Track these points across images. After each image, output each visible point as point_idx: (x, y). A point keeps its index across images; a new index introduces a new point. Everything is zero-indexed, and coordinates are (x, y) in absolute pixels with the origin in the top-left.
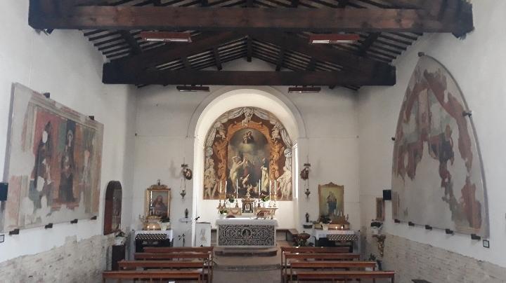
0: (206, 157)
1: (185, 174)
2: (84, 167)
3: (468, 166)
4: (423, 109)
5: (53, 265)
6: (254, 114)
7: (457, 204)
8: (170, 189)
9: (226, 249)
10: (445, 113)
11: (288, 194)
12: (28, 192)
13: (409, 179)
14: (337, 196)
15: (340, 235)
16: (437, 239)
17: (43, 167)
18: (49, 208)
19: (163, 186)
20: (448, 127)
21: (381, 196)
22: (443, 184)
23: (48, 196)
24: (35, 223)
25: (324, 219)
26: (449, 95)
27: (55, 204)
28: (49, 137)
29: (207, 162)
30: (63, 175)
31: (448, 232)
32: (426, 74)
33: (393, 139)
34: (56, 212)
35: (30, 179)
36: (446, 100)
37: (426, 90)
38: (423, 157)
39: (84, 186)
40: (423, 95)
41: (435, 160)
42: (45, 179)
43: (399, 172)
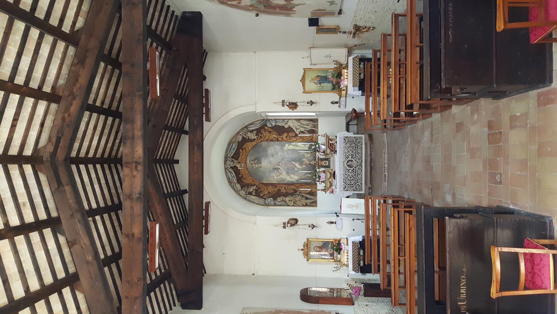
0: (275, 205)
6: (232, 157)
8: (308, 239)
9: (366, 184)
11: (311, 123)
14: (314, 75)
15: (353, 65)
19: (304, 246)
21: (314, 28)
25: (337, 87)
33: (257, 15)
43: (291, 9)
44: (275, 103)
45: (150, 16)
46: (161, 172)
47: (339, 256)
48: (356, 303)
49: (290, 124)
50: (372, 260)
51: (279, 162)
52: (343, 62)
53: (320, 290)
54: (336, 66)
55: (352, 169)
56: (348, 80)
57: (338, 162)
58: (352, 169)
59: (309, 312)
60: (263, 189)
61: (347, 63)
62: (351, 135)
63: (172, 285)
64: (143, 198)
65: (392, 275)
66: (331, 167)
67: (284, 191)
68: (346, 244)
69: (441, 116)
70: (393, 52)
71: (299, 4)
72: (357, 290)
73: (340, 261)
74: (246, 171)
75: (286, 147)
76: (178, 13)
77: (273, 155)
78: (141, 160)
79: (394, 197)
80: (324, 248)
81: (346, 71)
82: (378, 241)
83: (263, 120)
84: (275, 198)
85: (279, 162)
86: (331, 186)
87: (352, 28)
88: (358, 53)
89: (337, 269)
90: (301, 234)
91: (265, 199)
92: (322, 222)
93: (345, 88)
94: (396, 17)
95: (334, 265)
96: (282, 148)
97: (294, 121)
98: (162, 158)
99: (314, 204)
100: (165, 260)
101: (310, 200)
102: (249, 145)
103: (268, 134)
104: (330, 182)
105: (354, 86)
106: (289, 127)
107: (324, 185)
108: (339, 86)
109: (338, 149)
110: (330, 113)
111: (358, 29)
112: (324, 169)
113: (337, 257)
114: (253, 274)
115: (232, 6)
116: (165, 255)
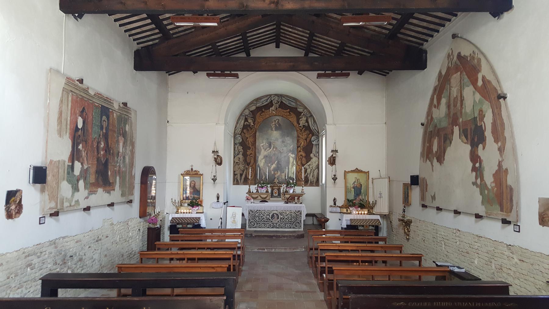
0: (235, 144)
1: (216, 160)
2: (119, 152)
3: (501, 150)
4: (455, 92)
5: (92, 245)
6: (282, 102)
7: (487, 189)
8: (202, 175)
9: (255, 231)
10: (478, 96)
11: (315, 180)
12: (66, 175)
13: (438, 164)
14: (363, 182)
15: (372, 220)
16: (466, 223)
17: (79, 151)
18: (87, 191)
19: (195, 171)
20: (481, 111)
21: (408, 181)
22: (474, 169)
23: (85, 180)
24: (73, 208)
25: (350, 204)
26: (483, 77)
27: (92, 188)
28: (84, 123)
29: (236, 149)
30: (98, 159)
31: (478, 216)
32: (459, 55)
33: (422, 124)
34: (93, 195)
35: (67, 163)
36: (480, 83)
37: (459, 73)
38: (453, 142)
39: (119, 170)
40: (455, 78)
41: (466, 145)
42: (82, 164)
43: (428, 157)
44: (335, 143)
45: (423, 17)
46: (267, 30)
47: (186, 205)
48: (142, 220)
49: (314, 159)
50: (183, 235)
51: (277, 150)
52: (375, 210)
53: (153, 188)
54: (371, 203)
55: (270, 218)
56: (357, 215)
57: (276, 205)
58: (270, 218)
59: (133, 174)
60: (251, 132)
61: (374, 214)
62: (303, 217)
63: (157, 41)
64: (243, 9)
65: (169, 252)
66: (271, 199)
67: (248, 153)
68: (198, 211)
69: (322, 301)
70: (384, 255)
71: (433, 166)
72: (154, 221)
73: (181, 205)
74: (267, 116)
75: (291, 155)
76: (426, 46)
77: (283, 142)
78: (280, 7)
79: (243, 256)
80: (194, 191)
81: (366, 212)
82: (201, 240)
83: (318, 132)
84: (241, 144)
85: (276, 148)
86: (254, 198)
87: (408, 218)
88: (384, 225)
89: (174, 203)
90: (207, 169)
91: (240, 134)
92: (219, 189)
93: (349, 211)
94: (419, 258)
95: (178, 200)
96: (290, 151)
97: (317, 163)
98: (281, 31)
99: (236, 182)
100: (182, 34)
101: (240, 178)
102: (293, 119)
103: (304, 137)
104: (257, 197)
105: (351, 220)
106: (311, 158)
107: (255, 191)
108: (351, 207)
109: (289, 205)
110: (325, 197)
111: (407, 224)
112: (270, 191)
113: (185, 203)
114: (168, 122)
115: (432, 99)
116: (186, 34)
